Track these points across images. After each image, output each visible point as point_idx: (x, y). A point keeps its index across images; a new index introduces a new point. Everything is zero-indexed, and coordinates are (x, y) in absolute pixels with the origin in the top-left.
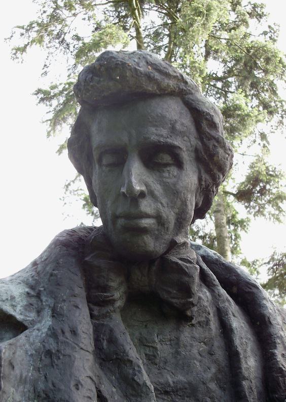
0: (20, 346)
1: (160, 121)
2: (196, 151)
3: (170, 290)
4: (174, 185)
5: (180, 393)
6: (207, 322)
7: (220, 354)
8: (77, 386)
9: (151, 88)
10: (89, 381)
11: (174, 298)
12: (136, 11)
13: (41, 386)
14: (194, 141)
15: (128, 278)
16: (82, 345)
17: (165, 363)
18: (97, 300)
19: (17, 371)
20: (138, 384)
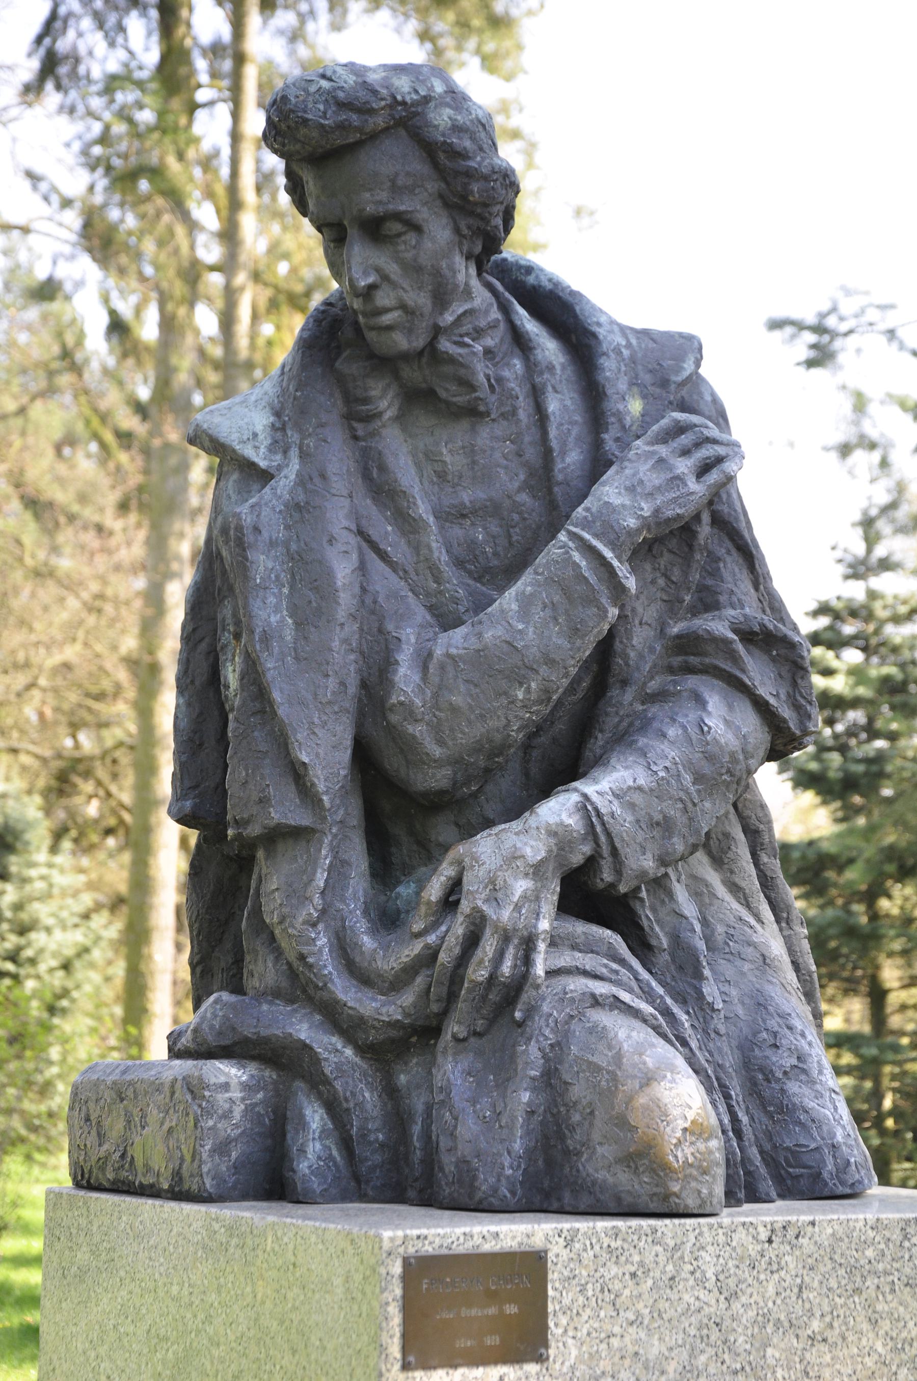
0: (266, 504)
2: (441, 196)
3: (448, 386)
4: (415, 260)
5: (481, 513)
6: (514, 412)
7: (531, 454)
8: (331, 541)
10: (345, 533)
11: (455, 396)
13: (294, 547)
15: (397, 376)
16: (334, 491)
17: (460, 477)
18: (357, 416)
19: (265, 534)
20: (414, 520)
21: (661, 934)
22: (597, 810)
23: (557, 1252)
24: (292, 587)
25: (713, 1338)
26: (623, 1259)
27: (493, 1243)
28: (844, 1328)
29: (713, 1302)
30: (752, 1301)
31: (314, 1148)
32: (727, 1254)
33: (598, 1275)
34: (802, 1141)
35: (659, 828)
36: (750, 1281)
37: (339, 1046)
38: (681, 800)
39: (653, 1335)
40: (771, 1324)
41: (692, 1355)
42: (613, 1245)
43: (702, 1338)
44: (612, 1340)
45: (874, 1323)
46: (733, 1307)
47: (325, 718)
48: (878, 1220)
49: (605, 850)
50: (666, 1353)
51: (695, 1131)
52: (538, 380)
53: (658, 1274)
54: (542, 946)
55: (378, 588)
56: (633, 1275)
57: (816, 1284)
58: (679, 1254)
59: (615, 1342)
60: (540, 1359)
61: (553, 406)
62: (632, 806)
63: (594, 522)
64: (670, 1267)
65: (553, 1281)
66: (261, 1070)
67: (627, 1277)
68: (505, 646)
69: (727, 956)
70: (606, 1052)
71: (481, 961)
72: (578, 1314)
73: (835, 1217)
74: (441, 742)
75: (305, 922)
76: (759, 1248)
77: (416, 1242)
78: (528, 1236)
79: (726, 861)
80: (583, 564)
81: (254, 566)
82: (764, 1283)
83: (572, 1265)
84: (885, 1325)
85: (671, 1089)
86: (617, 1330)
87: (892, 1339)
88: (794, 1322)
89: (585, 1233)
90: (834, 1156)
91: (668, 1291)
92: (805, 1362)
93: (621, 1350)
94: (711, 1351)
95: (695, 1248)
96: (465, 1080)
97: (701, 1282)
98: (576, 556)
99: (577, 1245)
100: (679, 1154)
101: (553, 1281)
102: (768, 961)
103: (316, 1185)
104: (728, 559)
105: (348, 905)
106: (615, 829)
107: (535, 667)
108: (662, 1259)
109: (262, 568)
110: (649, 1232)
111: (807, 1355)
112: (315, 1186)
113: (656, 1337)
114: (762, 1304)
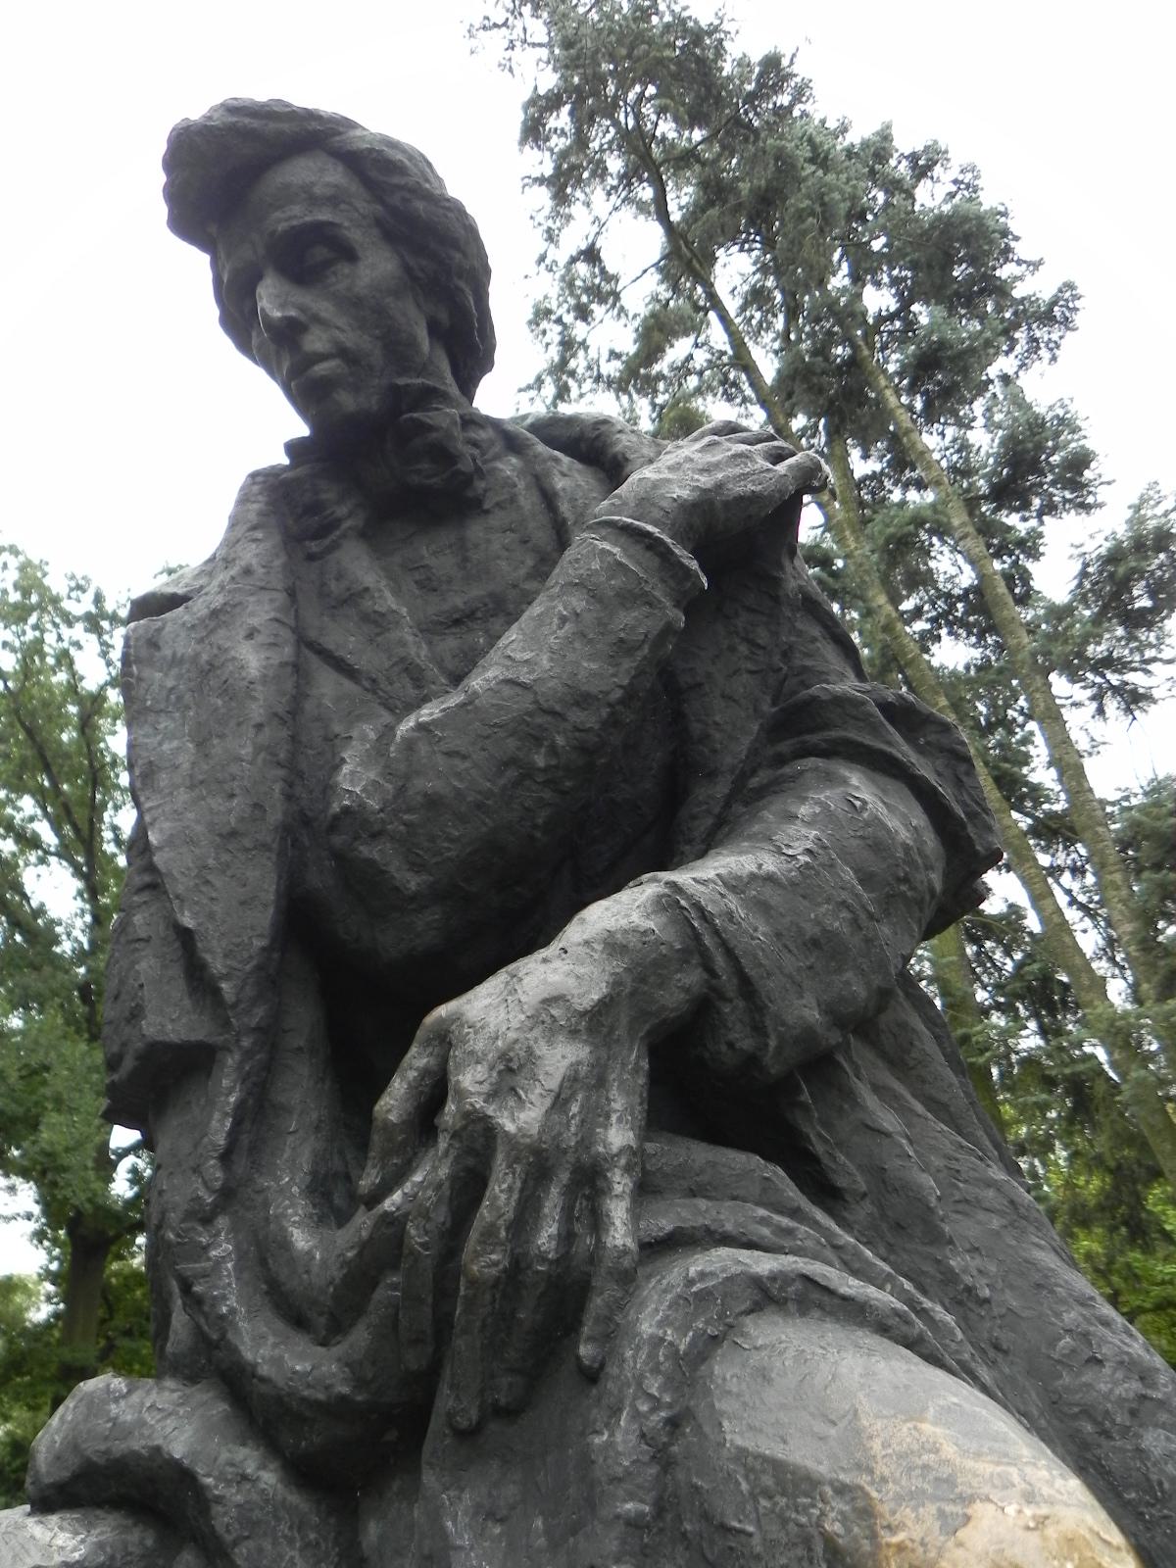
2: (378, 222)
3: (419, 466)
6: (513, 499)
12: (694, 262)
14: (364, 205)
19: (167, 652)
20: (383, 615)
38: (848, 907)
47: (225, 857)
54: (620, 1183)
62: (763, 907)
66: (126, 1529)
68: (507, 691)
69: (960, 1207)
74: (417, 867)
75: (189, 1215)
79: (912, 1063)
80: (616, 550)
96: (480, 1535)
102: (1022, 1210)
105: (278, 1179)
106: (740, 946)
107: (558, 708)
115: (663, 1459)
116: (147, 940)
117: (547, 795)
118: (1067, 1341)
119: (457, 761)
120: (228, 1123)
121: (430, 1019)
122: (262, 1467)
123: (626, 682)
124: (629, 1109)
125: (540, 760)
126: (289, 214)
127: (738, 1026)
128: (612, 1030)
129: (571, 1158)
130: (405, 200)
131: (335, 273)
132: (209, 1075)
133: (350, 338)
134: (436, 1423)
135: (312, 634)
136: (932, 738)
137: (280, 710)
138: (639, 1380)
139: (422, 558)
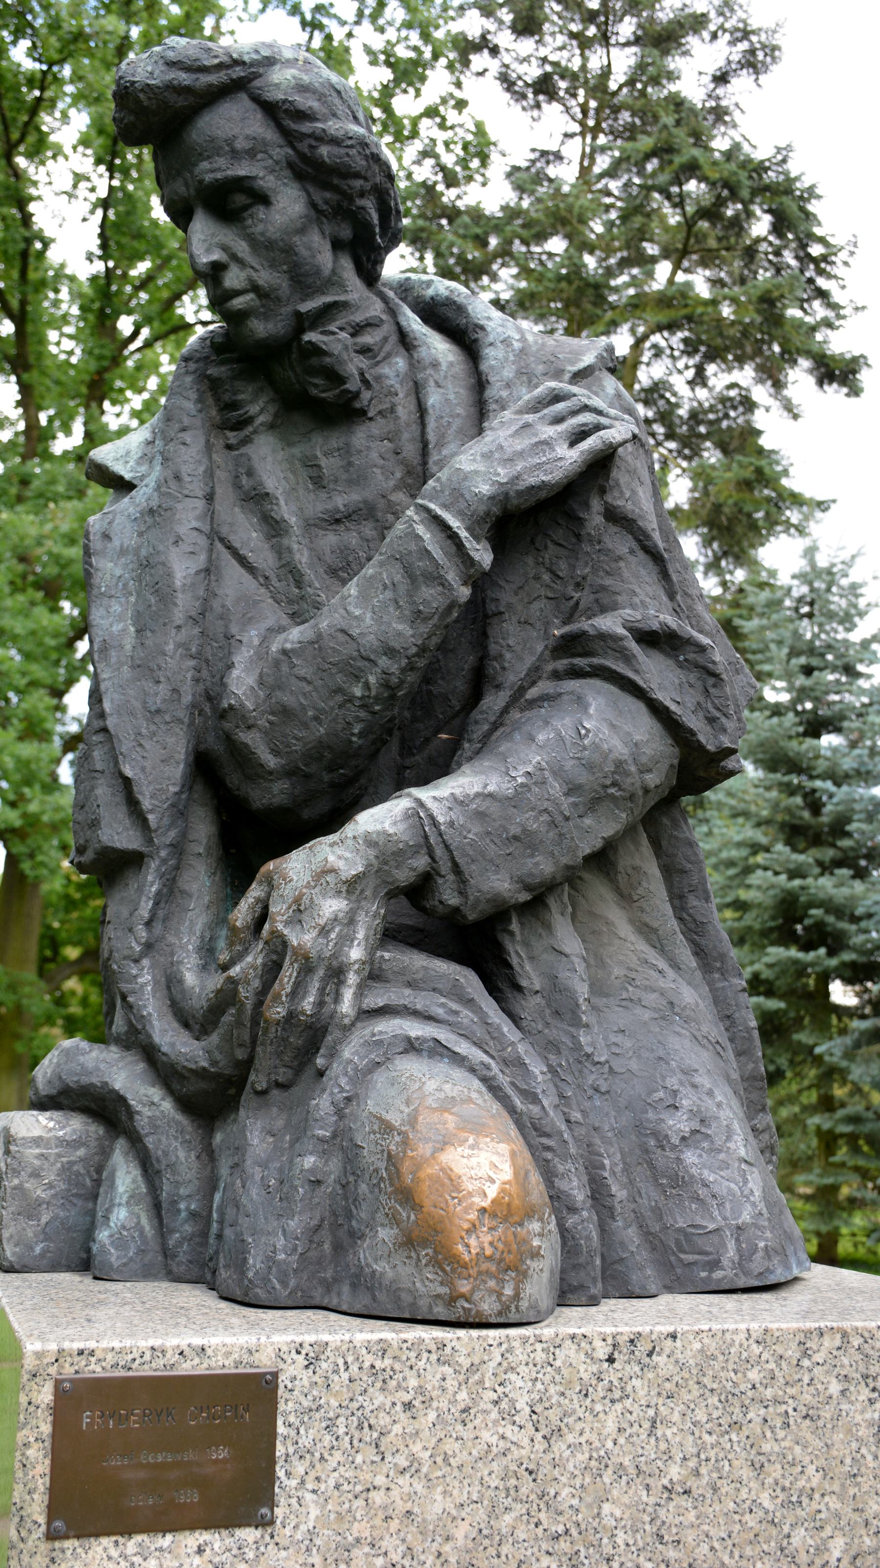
1: (213, 148)
2: (291, 165)
6: (392, 410)
9: (181, 102)
13: (144, 552)
15: (271, 382)
19: (116, 543)
20: (277, 522)
21: (532, 974)
22: (432, 818)
23: (293, 1373)
24: (139, 595)
25: (524, 1491)
26: (394, 1383)
27: (197, 1361)
28: (715, 1475)
29: (526, 1442)
30: (583, 1440)
31: (120, 1215)
32: (548, 1377)
33: (355, 1405)
34: (699, 1221)
35: (518, 844)
36: (580, 1413)
37: (156, 1099)
39: (434, 1487)
40: (610, 1471)
41: (493, 1512)
42: (379, 1364)
43: (507, 1490)
44: (372, 1494)
45: (759, 1468)
46: (555, 1448)
47: (153, 728)
48: (766, 1331)
49: (445, 866)
50: (454, 1512)
51: (502, 1212)
52: (420, 376)
53: (444, 1405)
54: (352, 979)
55: (229, 591)
56: (408, 1406)
57: (676, 1417)
58: (476, 1377)
59: (378, 1497)
60: (267, 1523)
61: (433, 399)
63: (442, 491)
64: (463, 1395)
65: (286, 1414)
67: (399, 1407)
69: (624, 1003)
70: (403, 1107)
71: (278, 996)
72: (322, 1458)
73: (705, 1327)
74: (275, 752)
76: (595, 1368)
77: (77, 1359)
78: (250, 1352)
79: (636, 898)
80: (427, 536)
81: (100, 574)
82: (601, 1415)
83: (315, 1393)
84: (775, 1471)
85: (469, 1156)
86: (380, 1480)
87: (783, 1489)
88: (643, 1467)
89: (337, 1349)
90: (737, 1240)
91: (459, 1427)
92: (659, 1523)
93: (385, 1508)
94: (520, 1509)
95: (502, 1369)
96: (263, 1141)
97: (510, 1415)
98: (420, 530)
99: (324, 1365)
100: (473, 1242)
101: (286, 1414)
103: (114, 1257)
104: (631, 558)
107: (372, 657)
108: (451, 1384)
109: (108, 576)
110: (433, 1348)
111: (662, 1513)
112: (113, 1259)
113: (440, 1489)
114: (597, 1444)
115: (340, 1114)
116: (102, 772)
117: (362, 714)
118: (661, 1094)
119: (304, 684)
120: (151, 903)
121: (263, 869)
122: (163, 1099)
123: (420, 642)
124: (367, 938)
125: (358, 692)
126: (215, 166)
127: (449, 891)
128: (362, 891)
129: (326, 963)
130: (311, 147)
131: (251, 216)
132: (140, 867)
133: (265, 277)
134: (248, 1087)
135: (224, 530)
136: (691, 656)
137: (193, 613)
138: (337, 1077)
139: (316, 457)
